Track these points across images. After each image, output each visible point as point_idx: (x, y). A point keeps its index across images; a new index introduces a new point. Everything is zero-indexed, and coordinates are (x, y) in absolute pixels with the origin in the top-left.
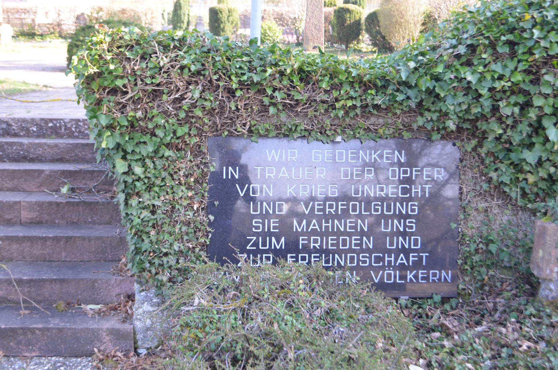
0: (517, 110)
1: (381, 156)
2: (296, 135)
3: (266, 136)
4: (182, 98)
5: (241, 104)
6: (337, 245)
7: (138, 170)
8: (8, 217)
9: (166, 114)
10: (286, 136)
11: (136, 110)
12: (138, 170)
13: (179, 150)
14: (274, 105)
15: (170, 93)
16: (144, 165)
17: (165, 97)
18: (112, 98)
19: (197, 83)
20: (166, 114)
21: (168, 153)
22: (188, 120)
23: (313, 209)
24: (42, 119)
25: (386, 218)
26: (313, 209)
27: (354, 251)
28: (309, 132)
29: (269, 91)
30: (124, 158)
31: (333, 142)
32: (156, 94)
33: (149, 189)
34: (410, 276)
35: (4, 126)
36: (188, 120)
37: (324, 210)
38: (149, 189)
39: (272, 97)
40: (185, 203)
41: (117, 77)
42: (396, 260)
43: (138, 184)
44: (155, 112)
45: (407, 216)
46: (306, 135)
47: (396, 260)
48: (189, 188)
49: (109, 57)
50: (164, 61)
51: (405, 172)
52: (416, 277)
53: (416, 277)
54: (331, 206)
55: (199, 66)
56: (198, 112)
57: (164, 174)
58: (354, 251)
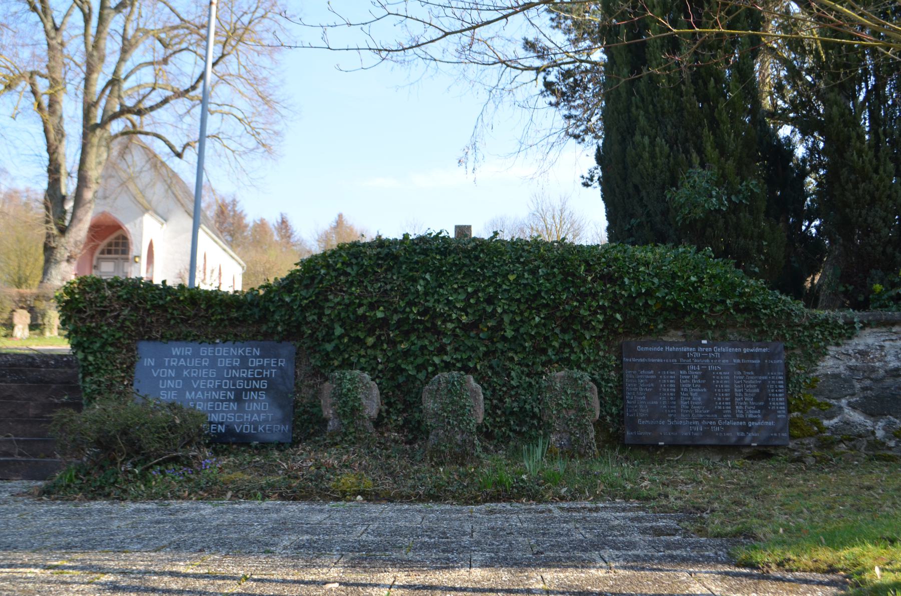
0: (315, 317)
1: (244, 351)
2: (190, 339)
3: (172, 340)
4: (119, 315)
5: (154, 319)
6: (213, 408)
7: (91, 358)
8: (20, 413)
9: (109, 325)
10: (185, 339)
11: (91, 322)
12: (91, 358)
13: (118, 348)
14: (174, 319)
15: (112, 311)
16: (95, 356)
17: (108, 314)
18: (78, 315)
19: (127, 306)
20: (109, 325)
21: (110, 349)
22: (121, 328)
23: (199, 385)
24: (59, 355)
25: (246, 390)
26: (199, 385)
27: (224, 412)
28: (199, 337)
29: (170, 311)
30: (83, 351)
31: (214, 343)
32: (103, 313)
33: (97, 372)
34: (260, 428)
35: (30, 360)
36: (121, 328)
37: (206, 386)
38: (97, 372)
39: (172, 314)
40: (119, 380)
41: (80, 302)
42: (252, 417)
43: (91, 368)
44: (103, 323)
45: (260, 389)
46: (195, 339)
47: (252, 417)
48: (123, 372)
49: (76, 291)
50: (108, 293)
51: (260, 361)
52: (264, 429)
53: (264, 429)
54: (211, 383)
55: (129, 296)
56: (128, 323)
57: (107, 362)
58: (224, 412)
